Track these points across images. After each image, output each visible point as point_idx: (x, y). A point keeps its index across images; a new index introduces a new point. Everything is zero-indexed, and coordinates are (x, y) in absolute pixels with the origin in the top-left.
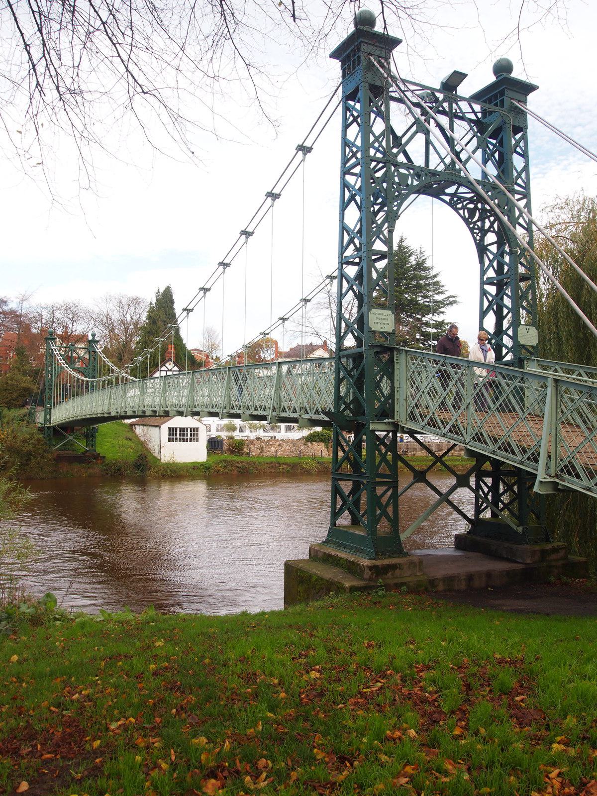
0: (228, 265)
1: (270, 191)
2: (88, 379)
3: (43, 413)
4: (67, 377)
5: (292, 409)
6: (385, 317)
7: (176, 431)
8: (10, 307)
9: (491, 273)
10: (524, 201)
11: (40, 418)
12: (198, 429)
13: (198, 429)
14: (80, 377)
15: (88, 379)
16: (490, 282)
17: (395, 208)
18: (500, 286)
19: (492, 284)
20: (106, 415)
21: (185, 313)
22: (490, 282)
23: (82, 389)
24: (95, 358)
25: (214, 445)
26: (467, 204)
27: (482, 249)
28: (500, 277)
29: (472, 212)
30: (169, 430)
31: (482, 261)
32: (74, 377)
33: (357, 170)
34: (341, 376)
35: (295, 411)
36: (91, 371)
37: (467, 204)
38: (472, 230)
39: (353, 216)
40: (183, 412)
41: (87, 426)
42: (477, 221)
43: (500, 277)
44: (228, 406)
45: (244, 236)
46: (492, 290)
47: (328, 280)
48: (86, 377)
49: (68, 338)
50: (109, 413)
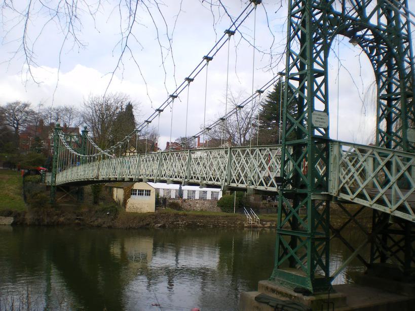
0: (192, 80)
1: (228, 29)
2: (79, 155)
3: (51, 177)
4: (68, 154)
5: (240, 181)
6: (322, 117)
7: (136, 191)
8: (30, 108)
9: (384, 92)
10: (408, 44)
11: (49, 179)
12: (150, 191)
13: (150, 191)
14: (77, 154)
15: (79, 155)
16: (383, 98)
17: (329, 41)
18: (390, 100)
19: (384, 99)
20: (95, 180)
21: (158, 112)
22: (383, 98)
23: (76, 161)
24: (85, 142)
25: (160, 202)
26: (369, 43)
27: (378, 75)
28: (389, 95)
29: (372, 49)
30: (150, 194)
31: (378, 83)
32: (73, 154)
33: (298, 15)
34: (286, 159)
35: (198, 179)
36: (83, 150)
37: (369, 43)
38: (372, 61)
39: (296, 47)
40: (153, 180)
41: (101, 187)
42: (375, 55)
43: (389, 95)
44: (188, 177)
45: (205, 60)
46: (385, 102)
47: (258, 93)
48: (78, 153)
49: (66, 130)
50: (98, 178)
